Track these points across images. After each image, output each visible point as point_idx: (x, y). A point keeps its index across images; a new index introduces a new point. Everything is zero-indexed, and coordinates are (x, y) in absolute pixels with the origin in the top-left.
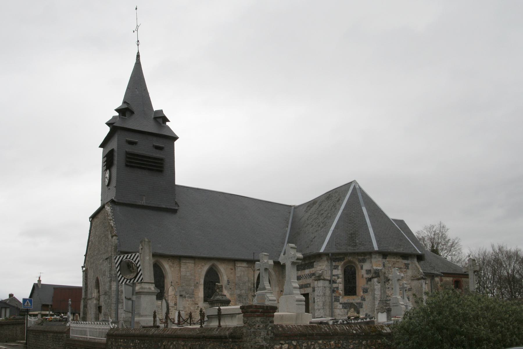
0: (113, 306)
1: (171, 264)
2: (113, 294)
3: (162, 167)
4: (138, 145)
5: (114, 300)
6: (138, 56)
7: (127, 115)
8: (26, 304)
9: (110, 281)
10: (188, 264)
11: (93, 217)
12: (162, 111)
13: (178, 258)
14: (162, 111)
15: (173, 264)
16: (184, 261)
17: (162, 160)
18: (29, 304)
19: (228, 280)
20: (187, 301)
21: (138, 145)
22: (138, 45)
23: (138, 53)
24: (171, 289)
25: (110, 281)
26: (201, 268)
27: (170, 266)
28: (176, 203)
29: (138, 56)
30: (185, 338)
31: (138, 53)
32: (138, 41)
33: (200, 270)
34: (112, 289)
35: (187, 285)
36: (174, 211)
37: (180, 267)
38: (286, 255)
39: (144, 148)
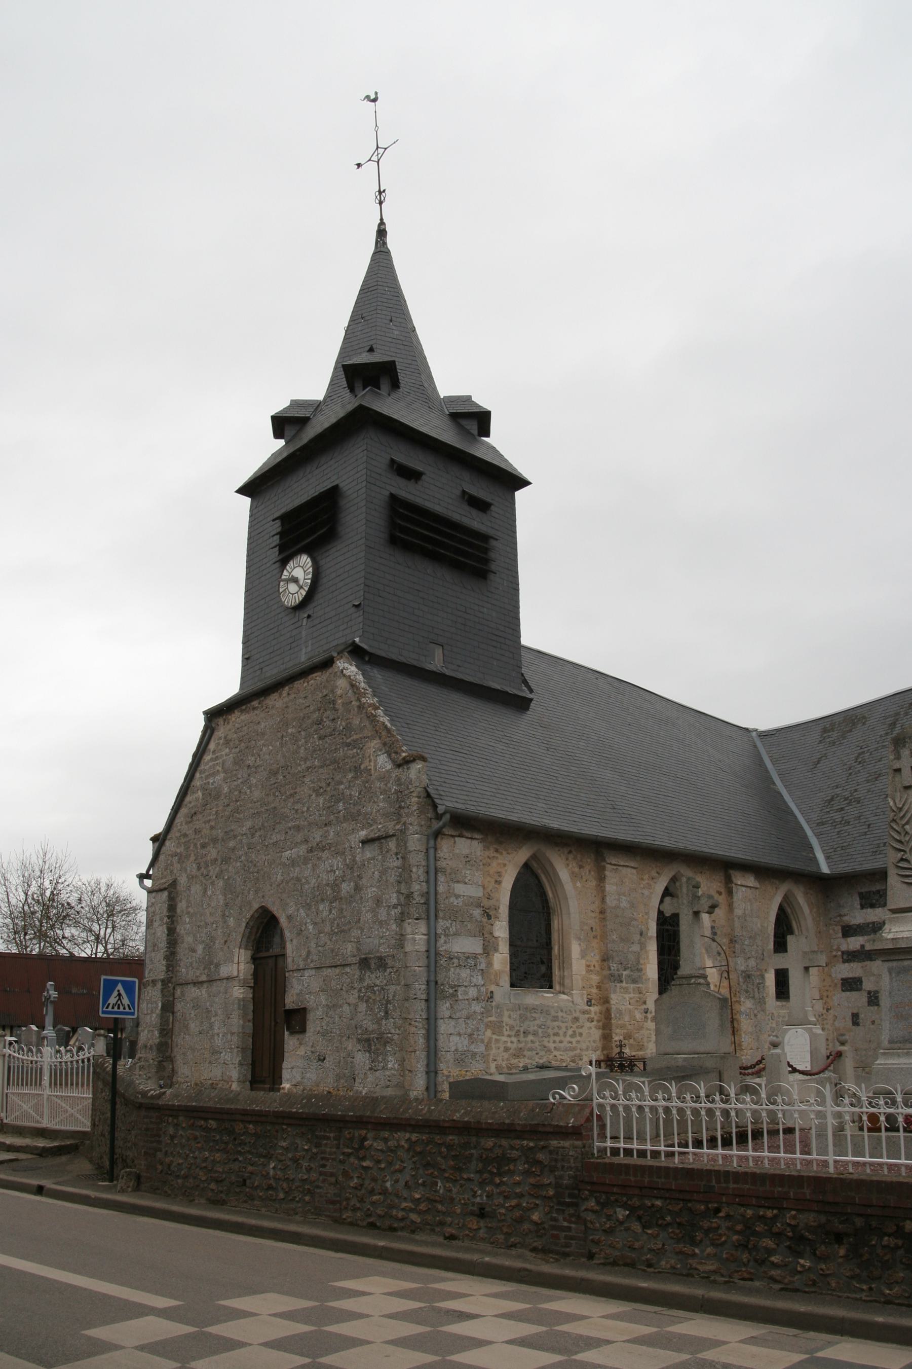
0: (418, 1010)
1: (574, 866)
2: (417, 966)
3: (487, 561)
4: (383, 500)
5: (419, 988)
6: (381, 233)
7: (382, 386)
8: (113, 1000)
9: (401, 919)
10: (624, 871)
11: (214, 716)
12: (470, 397)
13: (596, 849)
14: (470, 397)
15: (581, 867)
16: (612, 859)
17: (485, 538)
18: (126, 1001)
19: (713, 928)
20: (626, 990)
21: (383, 500)
22: (381, 203)
23: (382, 223)
24: (575, 949)
25: (401, 919)
26: (649, 886)
27: (574, 876)
28: (525, 682)
29: (381, 233)
30: (195, 983)
31: (382, 223)
32: (380, 192)
33: (646, 892)
34: (409, 948)
35: (622, 940)
36: (521, 704)
37: (601, 879)
38: (370, 852)
39: (439, 492)
